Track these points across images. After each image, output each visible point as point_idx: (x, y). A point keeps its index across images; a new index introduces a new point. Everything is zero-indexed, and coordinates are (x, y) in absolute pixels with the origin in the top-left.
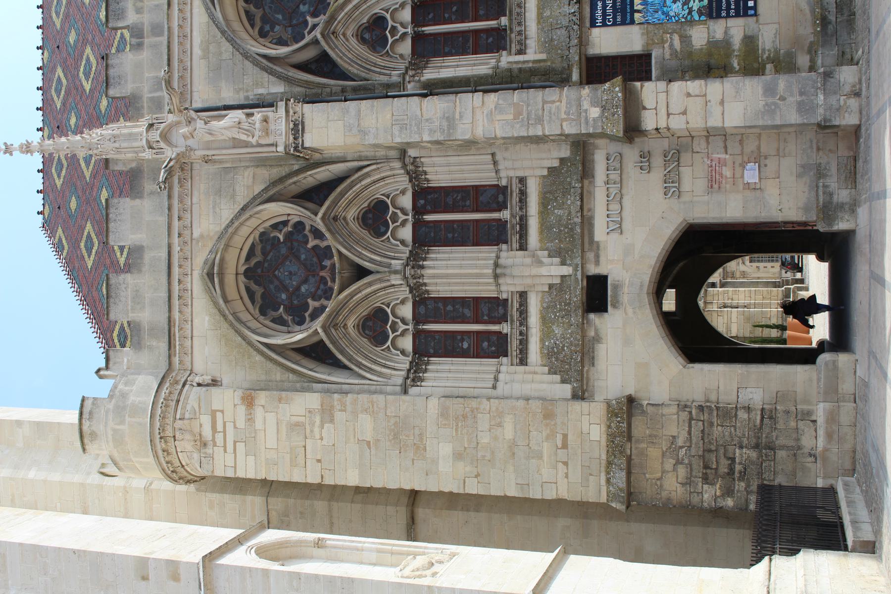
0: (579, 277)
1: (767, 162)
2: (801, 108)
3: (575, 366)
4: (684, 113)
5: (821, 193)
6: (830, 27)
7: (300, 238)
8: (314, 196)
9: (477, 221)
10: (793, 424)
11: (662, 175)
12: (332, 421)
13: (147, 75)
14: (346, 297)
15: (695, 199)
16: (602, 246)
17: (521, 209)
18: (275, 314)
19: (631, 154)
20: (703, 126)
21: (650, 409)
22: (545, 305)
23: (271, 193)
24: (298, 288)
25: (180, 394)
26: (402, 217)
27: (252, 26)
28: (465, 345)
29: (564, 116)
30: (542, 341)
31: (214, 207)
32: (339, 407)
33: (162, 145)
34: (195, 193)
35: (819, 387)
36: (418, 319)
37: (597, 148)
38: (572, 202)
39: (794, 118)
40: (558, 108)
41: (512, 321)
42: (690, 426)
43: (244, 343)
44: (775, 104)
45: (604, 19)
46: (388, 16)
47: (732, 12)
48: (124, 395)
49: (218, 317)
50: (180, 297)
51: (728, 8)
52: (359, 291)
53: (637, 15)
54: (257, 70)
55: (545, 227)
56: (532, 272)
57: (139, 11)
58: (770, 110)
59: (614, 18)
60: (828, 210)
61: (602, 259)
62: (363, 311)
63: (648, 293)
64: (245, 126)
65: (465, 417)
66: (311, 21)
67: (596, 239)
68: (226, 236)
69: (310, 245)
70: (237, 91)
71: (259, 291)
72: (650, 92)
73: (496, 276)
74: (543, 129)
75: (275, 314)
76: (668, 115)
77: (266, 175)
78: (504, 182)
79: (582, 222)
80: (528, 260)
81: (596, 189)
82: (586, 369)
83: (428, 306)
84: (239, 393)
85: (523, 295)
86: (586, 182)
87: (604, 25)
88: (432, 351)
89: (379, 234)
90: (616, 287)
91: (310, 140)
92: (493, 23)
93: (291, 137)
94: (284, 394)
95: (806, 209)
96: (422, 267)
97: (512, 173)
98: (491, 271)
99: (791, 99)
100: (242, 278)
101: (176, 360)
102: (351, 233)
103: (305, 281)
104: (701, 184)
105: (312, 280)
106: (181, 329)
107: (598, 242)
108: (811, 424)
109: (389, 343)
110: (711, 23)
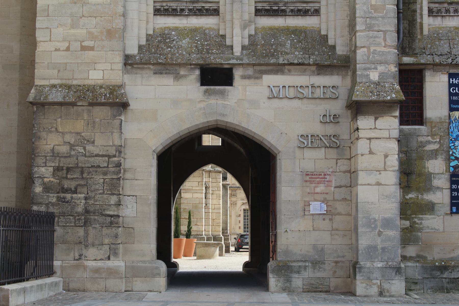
0: (234, 61)
1: (327, 221)
2: (372, 249)
4: (371, 152)
5: (300, 264)
6: (439, 273)
10: (106, 241)
15: (297, 161)
16: (258, 81)
17: (292, 11)
19: (337, 107)
20: (359, 168)
21: (117, 122)
22: (207, 31)
29: (372, 49)
30: (176, 29)
37: (344, 77)
38: (297, 56)
39: (363, 242)
40: (379, 44)
42: (103, 156)
44: (375, 227)
55: (275, 32)
58: (371, 223)
60: (286, 270)
61: (247, 82)
63: (217, 121)
67: (265, 77)
72: (390, 123)
74: (361, 31)
76: (370, 139)
79: (279, 65)
81: (307, 77)
82: (152, 67)
87: (450, 85)
90: (222, 93)
95: (287, 252)
99: (379, 240)
104: (309, 166)
107: (261, 78)
108: (107, 256)
110: (447, 176)
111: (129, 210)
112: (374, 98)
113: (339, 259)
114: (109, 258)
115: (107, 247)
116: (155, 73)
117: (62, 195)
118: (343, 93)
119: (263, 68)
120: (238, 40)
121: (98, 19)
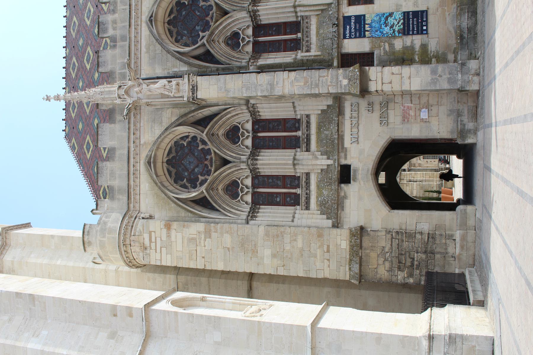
0: (336, 164)
2: (450, 81)
3: (334, 210)
4: (391, 83)
5: (459, 124)
6: (465, 40)
7: (195, 144)
8: (202, 123)
9: (285, 136)
10: (444, 241)
12: (210, 237)
13: (118, 61)
14: (218, 174)
15: (396, 126)
16: (348, 150)
17: (307, 130)
19: (363, 103)
20: (400, 89)
21: (372, 233)
22: (319, 180)
23: (180, 121)
24: (193, 170)
25: (133, 223)
26: (247, 134)
27: (172, 37)
28: (278, 200)
30: (317, 198)
31: (151, 128)
32: (213, 230)
33: (125, 96)
35: (457, 222)
37: (346, 100)
38: (333, 127)
39: (446, 86)
40: (327, 80)
41: (302, 188)
42: (392, 242)
43: (166, 197)
44: (437, 79)
49: (153, 184)
50: (134, 174)
51: (413, 30)
54: (174, 59)
56: (312, 162)
57: (114, 29)
58: (434, 82)
59: (355, 34)
60: (463, 133)
61: (348, 156)
62: (227, 182)
63: (371, 174)
64: (167, 87)
65: (278, 236)
69: (199, 148)
70: (164, 69)
71: (173, 171)
72: (373, 72)
73: (294, 165)
74: (319, 90)
75: (182, 183)
76: (382, 84)
78: (299, 117)
79: (338, 138)
80: (311, 157)
81: (346, 121)
82: (339, 212)
83: (259, 180)
84: (163, 223)
85: (308, 174)
87: (350, 37)
88: (261, 202)
90: (355, 171)
92: (294, 36)
93: (191, 93)
94: (186, 223)
95: (452, 132)
97: (303, 113)
98: (292, 157)
100: (165, 164)
101: (132, 205)
102: (221, 142)
103: (197, 166)
104: (399, 119)
105: (201, 166)
107: (346, 148)
109: (239, 198)
110: (405, 38)
112: (358, 82)
113: (456, 100)
117: (415, 267)
118: (355, 100)
119: (340, 147)
120: (324, 162)
121: (311, 242)
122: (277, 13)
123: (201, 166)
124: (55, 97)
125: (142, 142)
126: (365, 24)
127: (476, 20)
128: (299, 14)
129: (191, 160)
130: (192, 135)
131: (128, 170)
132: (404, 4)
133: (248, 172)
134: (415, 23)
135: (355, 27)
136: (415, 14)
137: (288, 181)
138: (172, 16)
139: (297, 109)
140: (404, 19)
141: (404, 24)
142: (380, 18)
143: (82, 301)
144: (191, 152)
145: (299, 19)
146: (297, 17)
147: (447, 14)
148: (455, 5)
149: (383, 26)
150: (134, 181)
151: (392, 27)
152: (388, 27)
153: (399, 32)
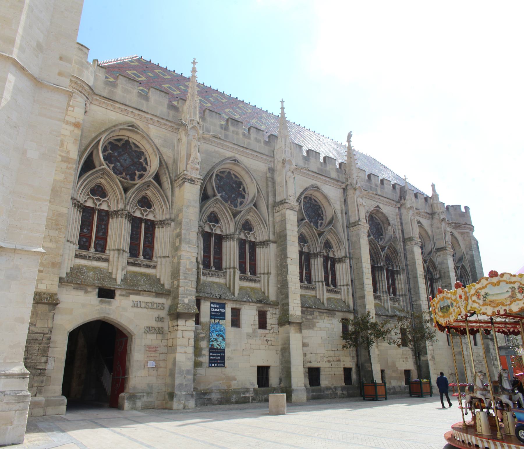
0: (116, 287)
1: (155, 371)
2: (181, 385)
3: (74, 279)
4: (183, 337)
5: (141, 394)
6: (203, 396)
7: (140, 168)
8: (157, 178)
10: (35, 385)
11: (153, 326)
12: (62, 161)
14: (117, 182)
17: (144, 265)
18: (109, 148)
19: (163, 314)
20: (177, 344)
21: (51, 314)
22: (102, 270)
23: (163, 162)
24: (119, 161)
25: (84, 94)
27: (220, 172)
28: (85, 230)
29: (186, 288)
30: (85, 266)
32: (69, 166)
34: (166, 131)
35: (51, 397)
36: (100, 211)
37: (167, 299)
38: (147, 287)
39: (177, 382)
40: (189, 286)
41: (96, 254)
42: (40, 333)
43: (101, 131)
45: (213, 307)
46: (106, 199)
47: (211, 357)
48: (87, 68)
49: (114, 124)
50: (126, 110)
51: (212, 356)
52: (119, 188)
53: (213, 320)
54: (208, 170)
55: (136, 274)
56: (117, 265)
57: (233, 132)
58: (181, 372)
59: (213, 312)
60: (133, 397)
61: (122, 298)
62: (107, 187)
65: (57, 225)
66: (112, 166)
68: (147, 137)
69: (136, 172)
71: (120, 144)
72: (191, 323)
73: (119, 250)
74: (182, 279)
75: (109, 148)
76: (183, 331)
77: (170, 162)
78: (155, 259)
79: (139, 290)
80: (124, 265)
82: (73, 285)
83: (105, 217)
84: (81, 122)
85: (107, 260)
86: (154, 294)
87: (211, 307)
88: (84, 214)
89: (139, 202)
90: (109, 303)
91: (187, 184)
92: (212, 264)
93: (189, 178)
94: (78, 142)
95: (134, 388)
96: (126, 218)
97: (159, 263)
98: (121, 248)
100: (126, 138)
101: (98, 98)
103: (121, 165)
104: (149, 343)
105: (122, 169)
106: (112, 105)
107: (129, 296)
108: (34, 394)
109: (91, 196)
110: (208, 349)
111: (50, 366)
112: (186, 311)
113: (159, 391)
114: (36, 395)
115: (35, 389)
116: (74, 289)
118: (167, 307)
119: (131, 291)
120: (119, 276)
121: (48, 256)
122: (230, 254)
123: (122, 169)
124: (195, 68)
125: (150, 125)
126: (219, 319)
127: (215, 405)
128: (228, 270)
129: (127, 162)
130: (148, 168)
131: (129, 106)
132: (230, 349)
133: (113, 208)
134: (217, 358)
135: (217, 312)
136: (223, 358)
137: (101, 242)
138: (233, 176)
139: (163, 259)
140: (220, 349)
141: (217, 349)
142: (222, 331)
143: (78, 32)
144: (134, 164)
145: (224, 270)
146: (226, 269)
147: (221, 382)
148: (226, 388)
149: (217, 333)
150: (120, 108)
151: (216, 340)
152: (216, 337)
153: (212, 345)
